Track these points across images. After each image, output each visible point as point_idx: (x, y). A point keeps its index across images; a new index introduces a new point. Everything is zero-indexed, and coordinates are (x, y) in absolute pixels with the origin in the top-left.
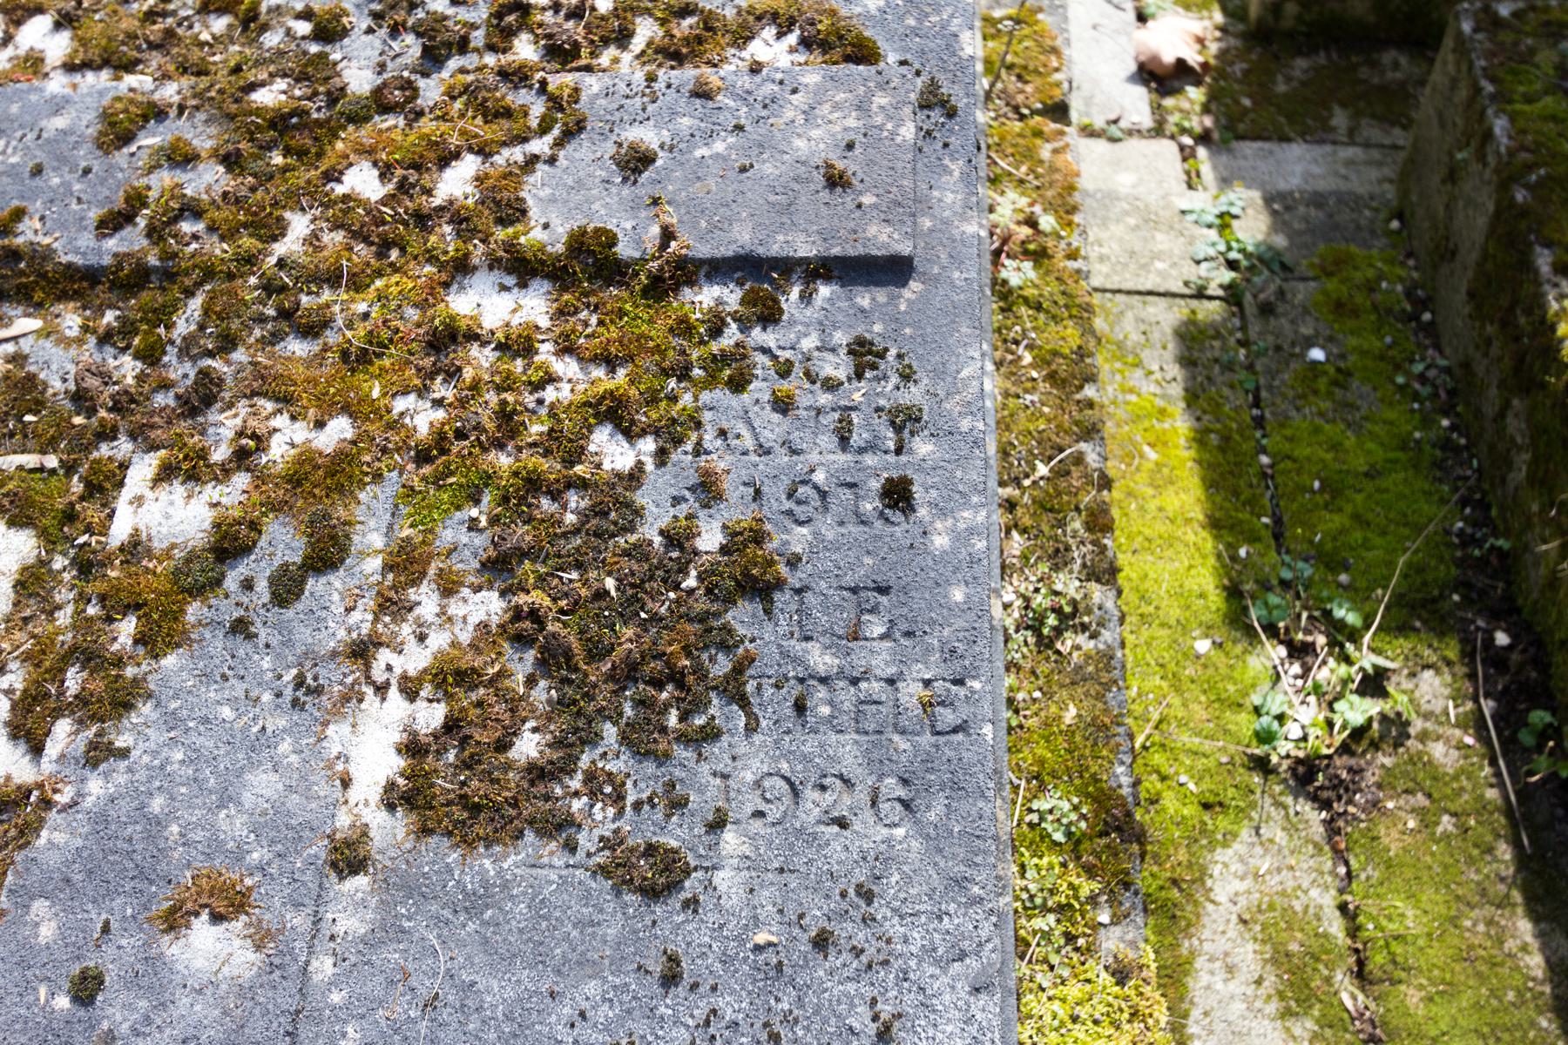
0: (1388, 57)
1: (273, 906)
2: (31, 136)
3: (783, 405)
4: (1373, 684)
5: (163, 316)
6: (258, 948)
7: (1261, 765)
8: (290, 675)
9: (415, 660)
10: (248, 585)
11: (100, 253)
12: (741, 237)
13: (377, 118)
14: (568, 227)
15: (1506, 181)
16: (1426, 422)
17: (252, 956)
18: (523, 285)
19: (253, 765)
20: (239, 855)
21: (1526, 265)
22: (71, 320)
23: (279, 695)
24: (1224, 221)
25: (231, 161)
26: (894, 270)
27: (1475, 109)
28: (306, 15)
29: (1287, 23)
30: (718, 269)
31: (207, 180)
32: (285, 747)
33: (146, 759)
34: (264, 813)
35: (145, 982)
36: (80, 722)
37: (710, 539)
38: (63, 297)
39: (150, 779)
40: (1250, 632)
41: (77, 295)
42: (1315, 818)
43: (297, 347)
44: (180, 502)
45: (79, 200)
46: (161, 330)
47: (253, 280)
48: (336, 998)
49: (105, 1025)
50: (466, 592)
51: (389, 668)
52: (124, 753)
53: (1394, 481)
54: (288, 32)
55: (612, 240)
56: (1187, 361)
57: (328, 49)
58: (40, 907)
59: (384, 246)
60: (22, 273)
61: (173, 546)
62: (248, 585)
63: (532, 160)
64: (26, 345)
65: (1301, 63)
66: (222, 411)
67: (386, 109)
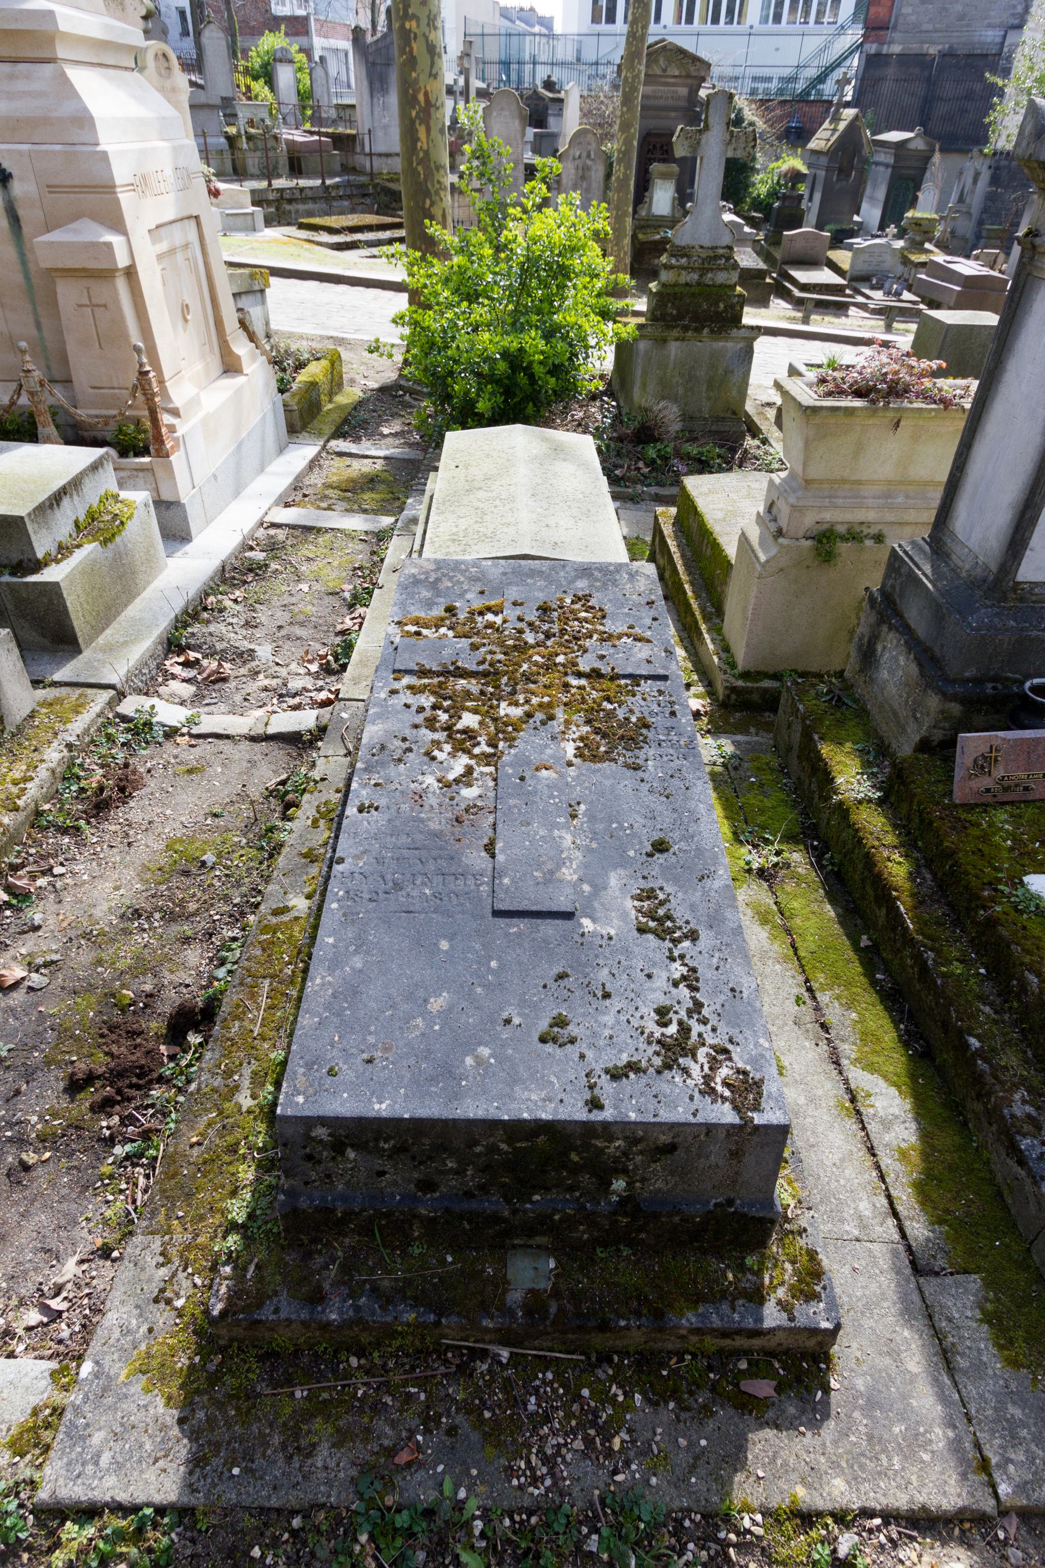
0: (767, 714)
3: (644, 699)
4: (778, 853)
7: (749, 871)
12: (629, 670)
15: (804, 720)
16: (788, 795)
21: (812, 739)
22: (474, 681)
24: (719, 747)
26: (664, 678)
27: (794, 705)
29: (732, 702)
30: (625, 677)
31: (501, 657)
37: (634, 719)
40: (741, 842)
42: (765, 885)
53: (781, 809)
56: (713, 780)
65: (738, 715)
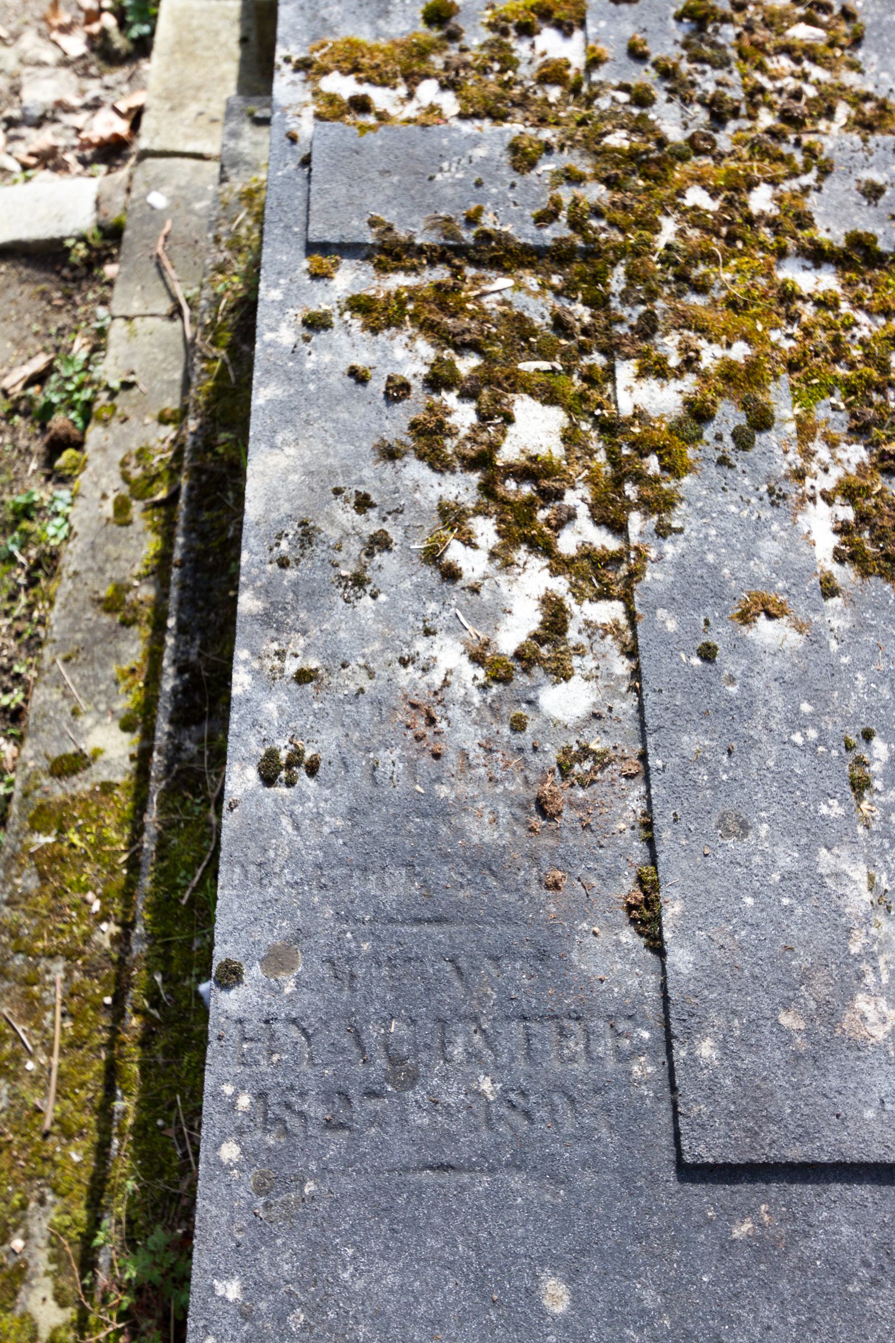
1: (800, 609)
2: (464, 161)
5: (599, 277)
6: (801, 632)
8: (764, 488)
9: (827, 483)
10: (719, 438)
11: (543, 238)
13: (694, 158)
14: (843, 231)
17: (800, 637)
18: (817, 266)
19: (759, 537)
20: (772, 585)
22: (532, 281)
23: (761, 499)
25: (610, 183)
28: (624, 88)
32: (775, 527)
33: (694, 534)
34: (777, 563)
35: (740, 650)
36: (645, 513)
38: (522, 265)
39: (701, 545)
41: (531, 265)
43: (693, 299)
44: (657, 390)
45: (515, 204)
46: (600, 287)
47: (655, 259)
48: (845, 660)
49: (726, 672)
50: (843, 445)
51: (812, 487)
52: (680, 531)
54: (613, 99)
55: (875, 240)
57: (645, 111)
58: (661, 613)
59: (731, 239)
60: (493, 249)
61: (663, 416)
62: (719, 438)
63: (805, 190)
64: (508, 295)
66: (662, 337)
67: (699, 152)
